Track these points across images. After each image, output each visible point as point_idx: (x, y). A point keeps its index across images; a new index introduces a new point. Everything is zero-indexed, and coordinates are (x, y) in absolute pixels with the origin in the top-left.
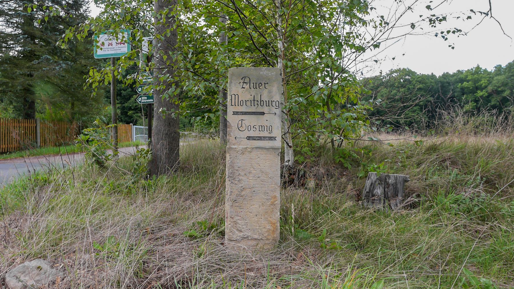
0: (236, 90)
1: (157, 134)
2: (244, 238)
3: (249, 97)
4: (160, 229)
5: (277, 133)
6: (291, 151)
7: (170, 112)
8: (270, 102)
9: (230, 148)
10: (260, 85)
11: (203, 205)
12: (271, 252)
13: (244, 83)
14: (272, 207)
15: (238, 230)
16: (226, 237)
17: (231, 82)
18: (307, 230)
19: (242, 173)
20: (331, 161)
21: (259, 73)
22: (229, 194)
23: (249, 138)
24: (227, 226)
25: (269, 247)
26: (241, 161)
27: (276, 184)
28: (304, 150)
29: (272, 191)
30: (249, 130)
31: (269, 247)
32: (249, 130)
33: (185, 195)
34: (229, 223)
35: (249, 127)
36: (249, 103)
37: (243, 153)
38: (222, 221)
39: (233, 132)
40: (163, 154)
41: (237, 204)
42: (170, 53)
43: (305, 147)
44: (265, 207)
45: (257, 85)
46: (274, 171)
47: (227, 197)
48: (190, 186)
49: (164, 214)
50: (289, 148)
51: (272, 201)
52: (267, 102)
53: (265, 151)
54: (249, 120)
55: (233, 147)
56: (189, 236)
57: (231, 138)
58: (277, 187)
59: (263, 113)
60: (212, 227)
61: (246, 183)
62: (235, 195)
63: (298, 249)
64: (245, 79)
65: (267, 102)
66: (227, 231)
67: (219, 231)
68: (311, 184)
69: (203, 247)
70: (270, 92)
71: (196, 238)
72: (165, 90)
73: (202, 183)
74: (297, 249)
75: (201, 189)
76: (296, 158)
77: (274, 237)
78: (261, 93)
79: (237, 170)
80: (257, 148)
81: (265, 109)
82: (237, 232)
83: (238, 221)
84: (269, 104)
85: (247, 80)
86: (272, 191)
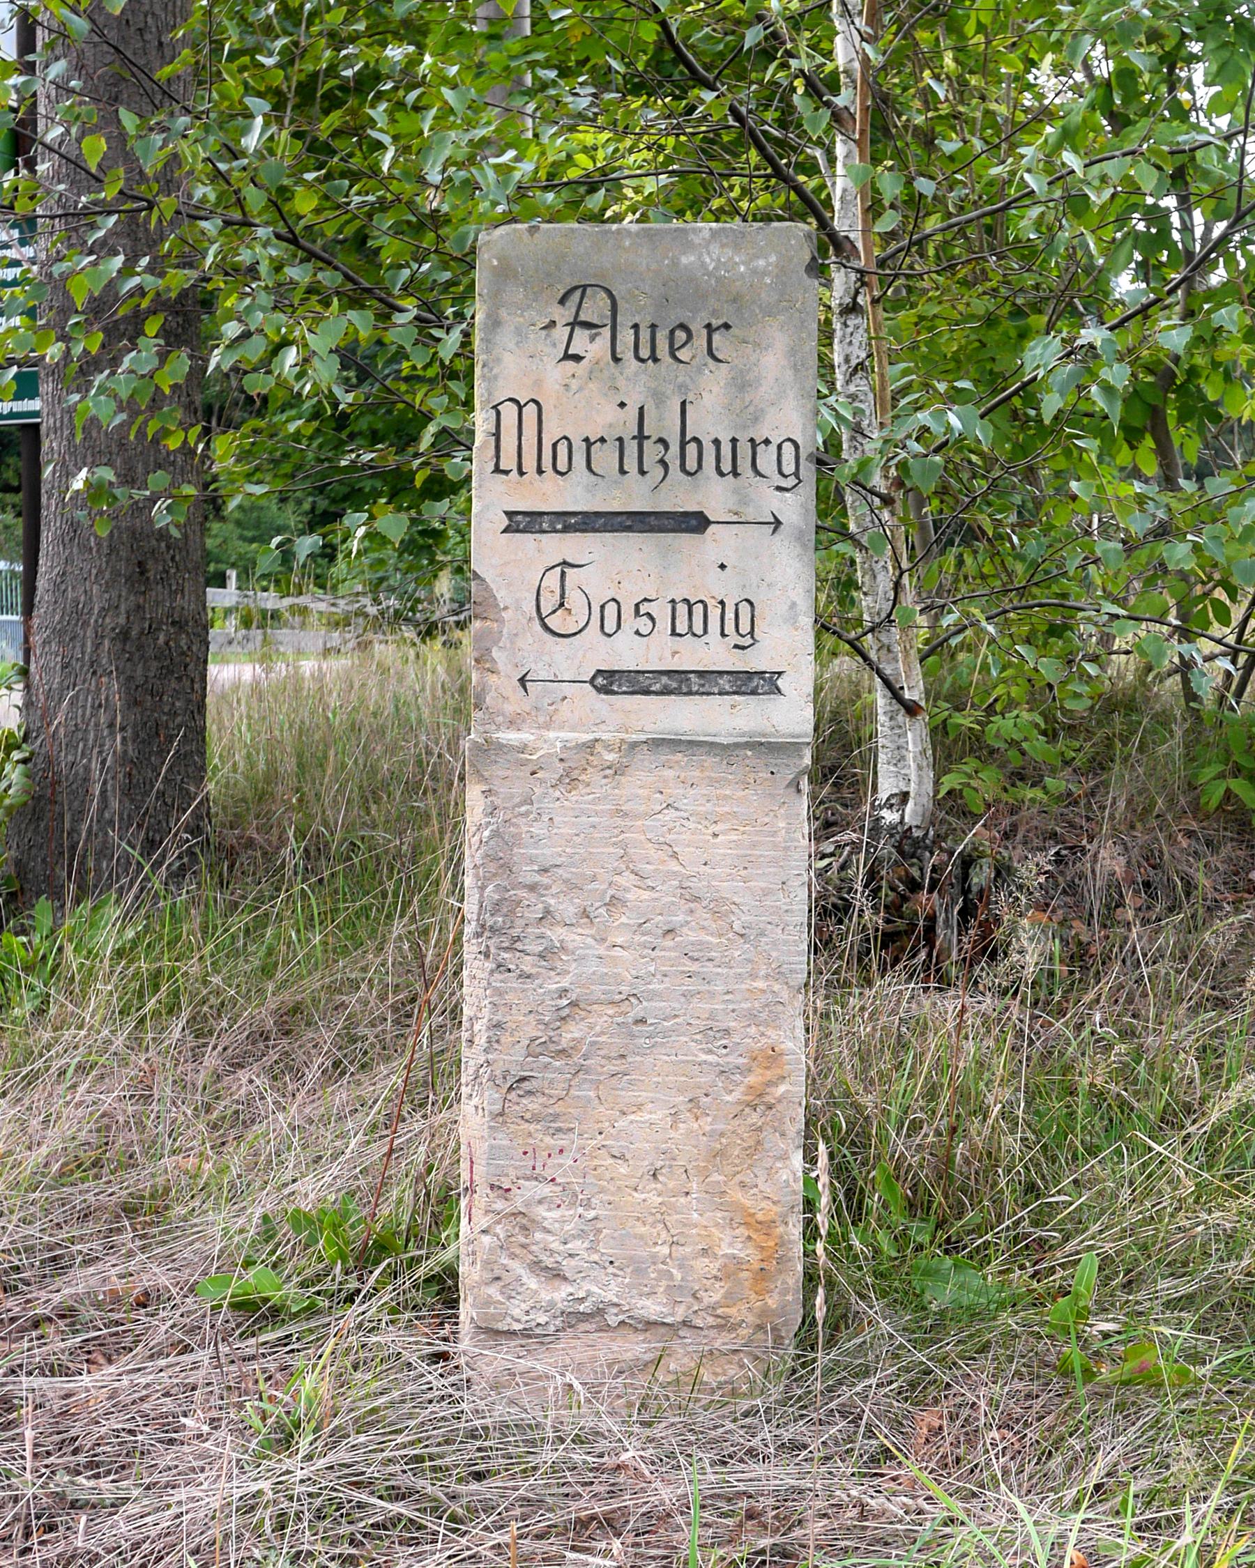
0: (531, 379)
1: (59, 633)
2: (573, 1319)
3: (605, 418)
4: (57, 1264)
5: (788, 645)
6: (915, 737)
7: (138, 495)
8: (744, 450)
9: (489, 748)
10: (681, 336)
11: (340, 1095)
12: (745, 1405)
13: (576, 323)
14: (754, 1118)
15: (536, 1266)
16: (466, 1311)
17: (494, 323)
18: (981, 1257)
19: (567, 908)
20: (1171, 801)
21: (675, 263)
22: (481, 1040)
23: (608, 681)
24: (472, 1242)
25: (732, 1371)
26: (559, 830)
27: (779, 974)
28: (1004, 725)
29: (752, 1017)
30: (610, 626)
31: (732, 1371)
32: (610, 626)
33: (230, 1033)
34: (483, 1221)
35: (611, 609)
36: (605, 458)
37: (569, 780)
38: (442, 1205)
39: (516, 645)
40: (100, 763)
41: (532, 1105)
42: (129, 120)
43: (1012, 704)
44: (706, 1123)
45: (662, 336)
46: (766, 893)
47: (472, 1058)
48: (267, 971)
49: (85, 1164)
50: (902, 717)
51: (751, 1079)
52: (726, 449)
53: (710, 761)
54: (611, 566)
55: (509, 736)
56: (235, 1306)
57: (492, 679)
58: (785, 995)
59: (697, 523)
60: (383, 1248)
61: (592, 967)
62: (520, 1050)
63: (918, 1387)
64: (582, 301)
65: (726, 449)
66: (469, 1273)
67: (421, 1272)
68: (1031, 947)
69: (312, 1384)
70: (742, 384)
71: (276, 1314)
72: (90, 365)
73: (345, 951)
74: (913, 1385)
75: (332, 989)
76: (949, 782)
77: (764, 1312)
78: (683, 388)
79: (532, 888)
80: (657, 744)
81: (713, 496)
82: (532, 1283)
83: (541, 1211)
84: (737, 459)
85: (596, 307)
86: (752, 1017)
